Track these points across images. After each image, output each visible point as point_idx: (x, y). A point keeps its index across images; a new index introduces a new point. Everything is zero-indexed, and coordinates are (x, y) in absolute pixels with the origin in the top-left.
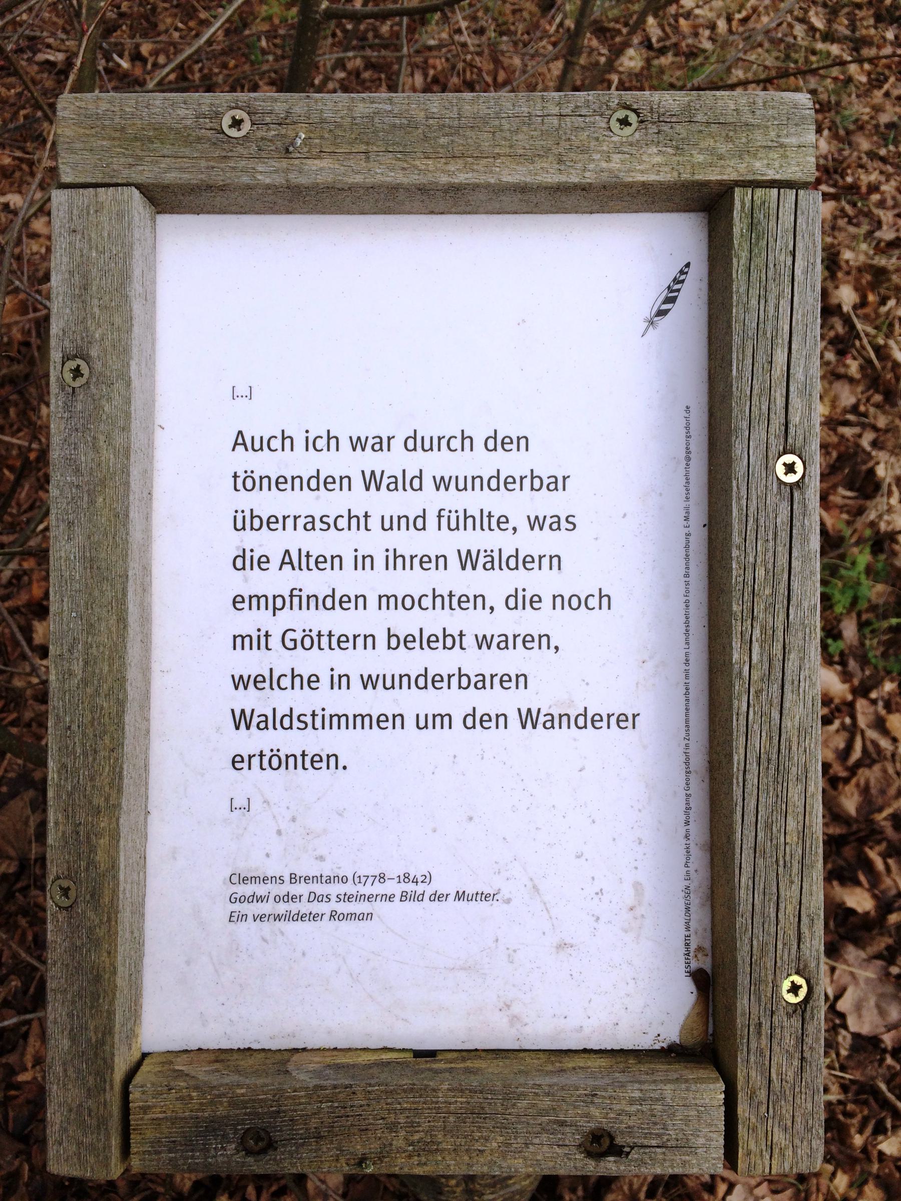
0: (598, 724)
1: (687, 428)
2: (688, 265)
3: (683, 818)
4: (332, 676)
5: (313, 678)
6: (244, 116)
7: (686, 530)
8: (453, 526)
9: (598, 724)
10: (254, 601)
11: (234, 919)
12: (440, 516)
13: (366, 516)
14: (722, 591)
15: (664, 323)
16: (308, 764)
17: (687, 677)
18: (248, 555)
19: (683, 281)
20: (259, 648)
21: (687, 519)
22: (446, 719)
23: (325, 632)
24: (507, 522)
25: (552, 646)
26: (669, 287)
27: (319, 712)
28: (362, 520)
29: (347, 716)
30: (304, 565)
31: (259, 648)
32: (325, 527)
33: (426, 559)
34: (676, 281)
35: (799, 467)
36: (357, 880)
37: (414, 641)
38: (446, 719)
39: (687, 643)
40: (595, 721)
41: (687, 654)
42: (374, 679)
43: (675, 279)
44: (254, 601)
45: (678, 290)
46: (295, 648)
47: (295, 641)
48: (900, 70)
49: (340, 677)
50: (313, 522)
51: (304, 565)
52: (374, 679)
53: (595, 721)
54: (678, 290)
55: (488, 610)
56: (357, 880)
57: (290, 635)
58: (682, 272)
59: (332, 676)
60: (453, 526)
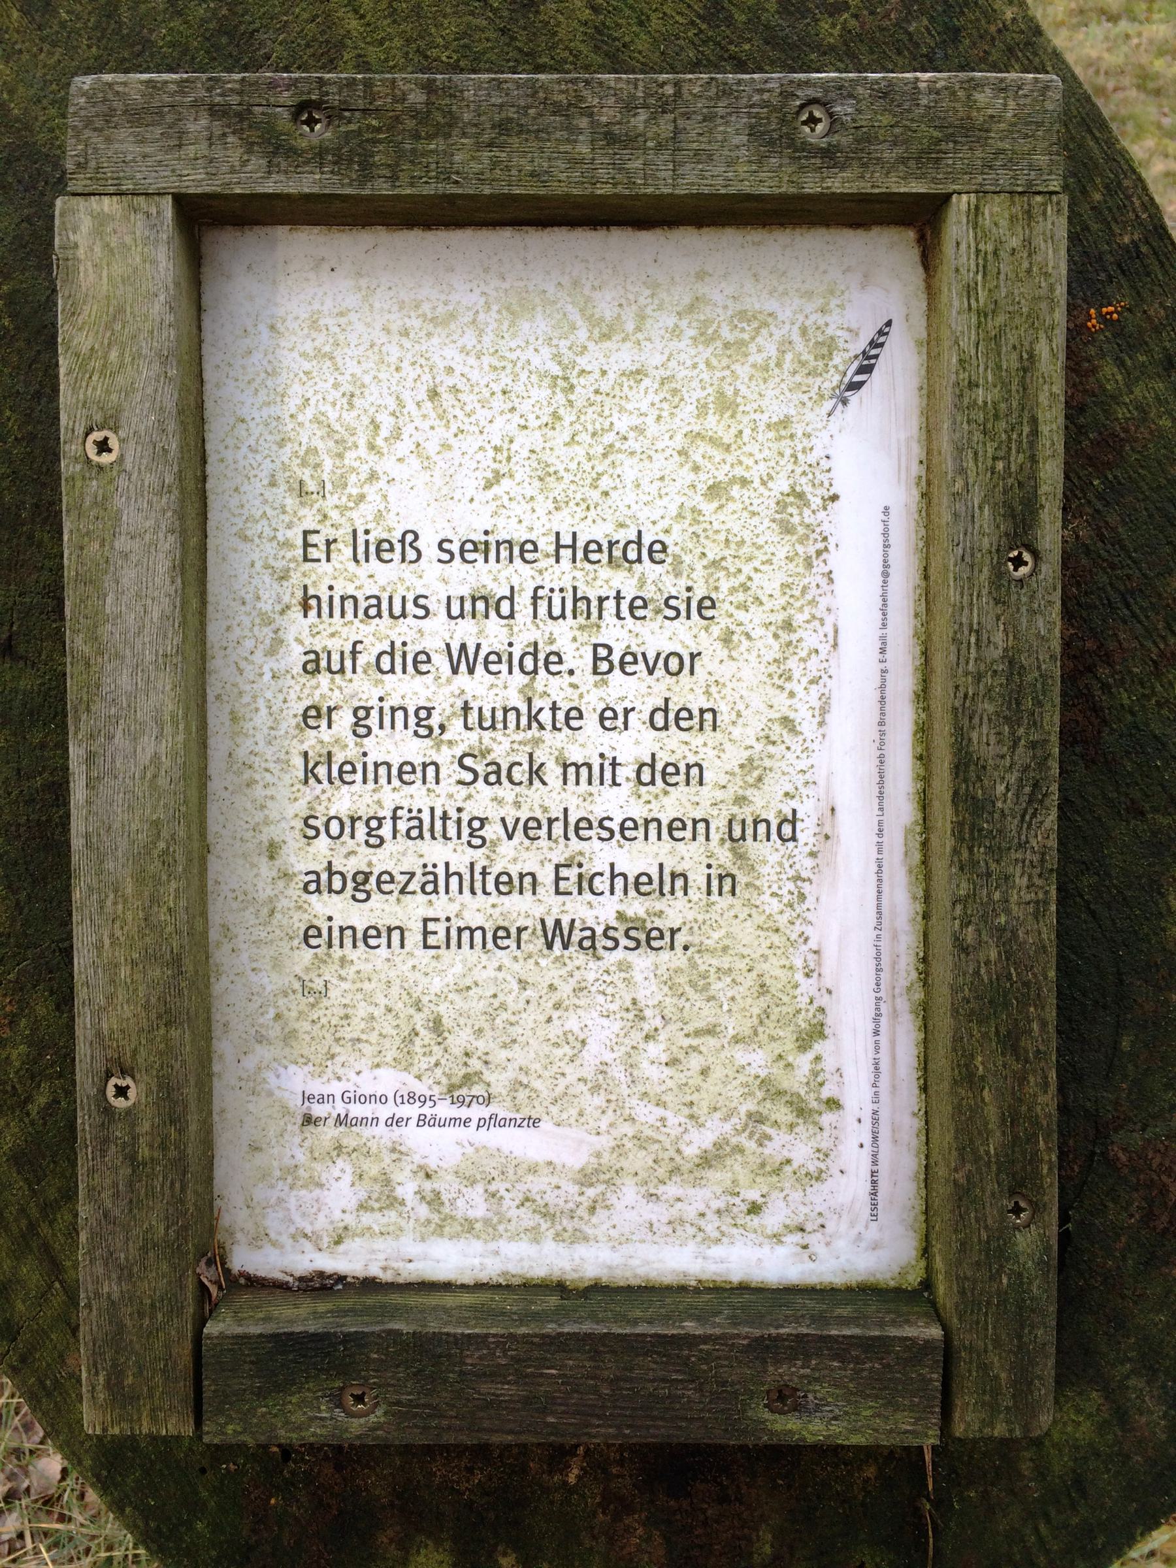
1: (886, 533)
2: (889, 324)
3: (871, 1026)
4: (709, 876)
7: (882, 666)
8: (556, 611)
11: (570, 885)
12: (535, 598)
14: (920, 758)
15: (854, 398)
16: (490, 887)
17: (880, 852)
19: (882, 345)
21: (883, 651)
24: (560, 662)
26: (864, 352)
27: (453, 814)
30: (478, 885)
32: (632, 944)
34: (874, 344)
35: (111, 1091)
36: (399, 1100)
39: (881, 809)
40: (883, 698)
41: (880, 823)
42: (471, 651)
43: (871, 343)
45: (876, 357)
48: (1175, 134)
51: (478, 885)
52: (471, 651)
53: (883, 698)
54: (876, 357)
56: (399, 1100)
58: (881, 333)
59: (709, 876)
60: (556, 611)
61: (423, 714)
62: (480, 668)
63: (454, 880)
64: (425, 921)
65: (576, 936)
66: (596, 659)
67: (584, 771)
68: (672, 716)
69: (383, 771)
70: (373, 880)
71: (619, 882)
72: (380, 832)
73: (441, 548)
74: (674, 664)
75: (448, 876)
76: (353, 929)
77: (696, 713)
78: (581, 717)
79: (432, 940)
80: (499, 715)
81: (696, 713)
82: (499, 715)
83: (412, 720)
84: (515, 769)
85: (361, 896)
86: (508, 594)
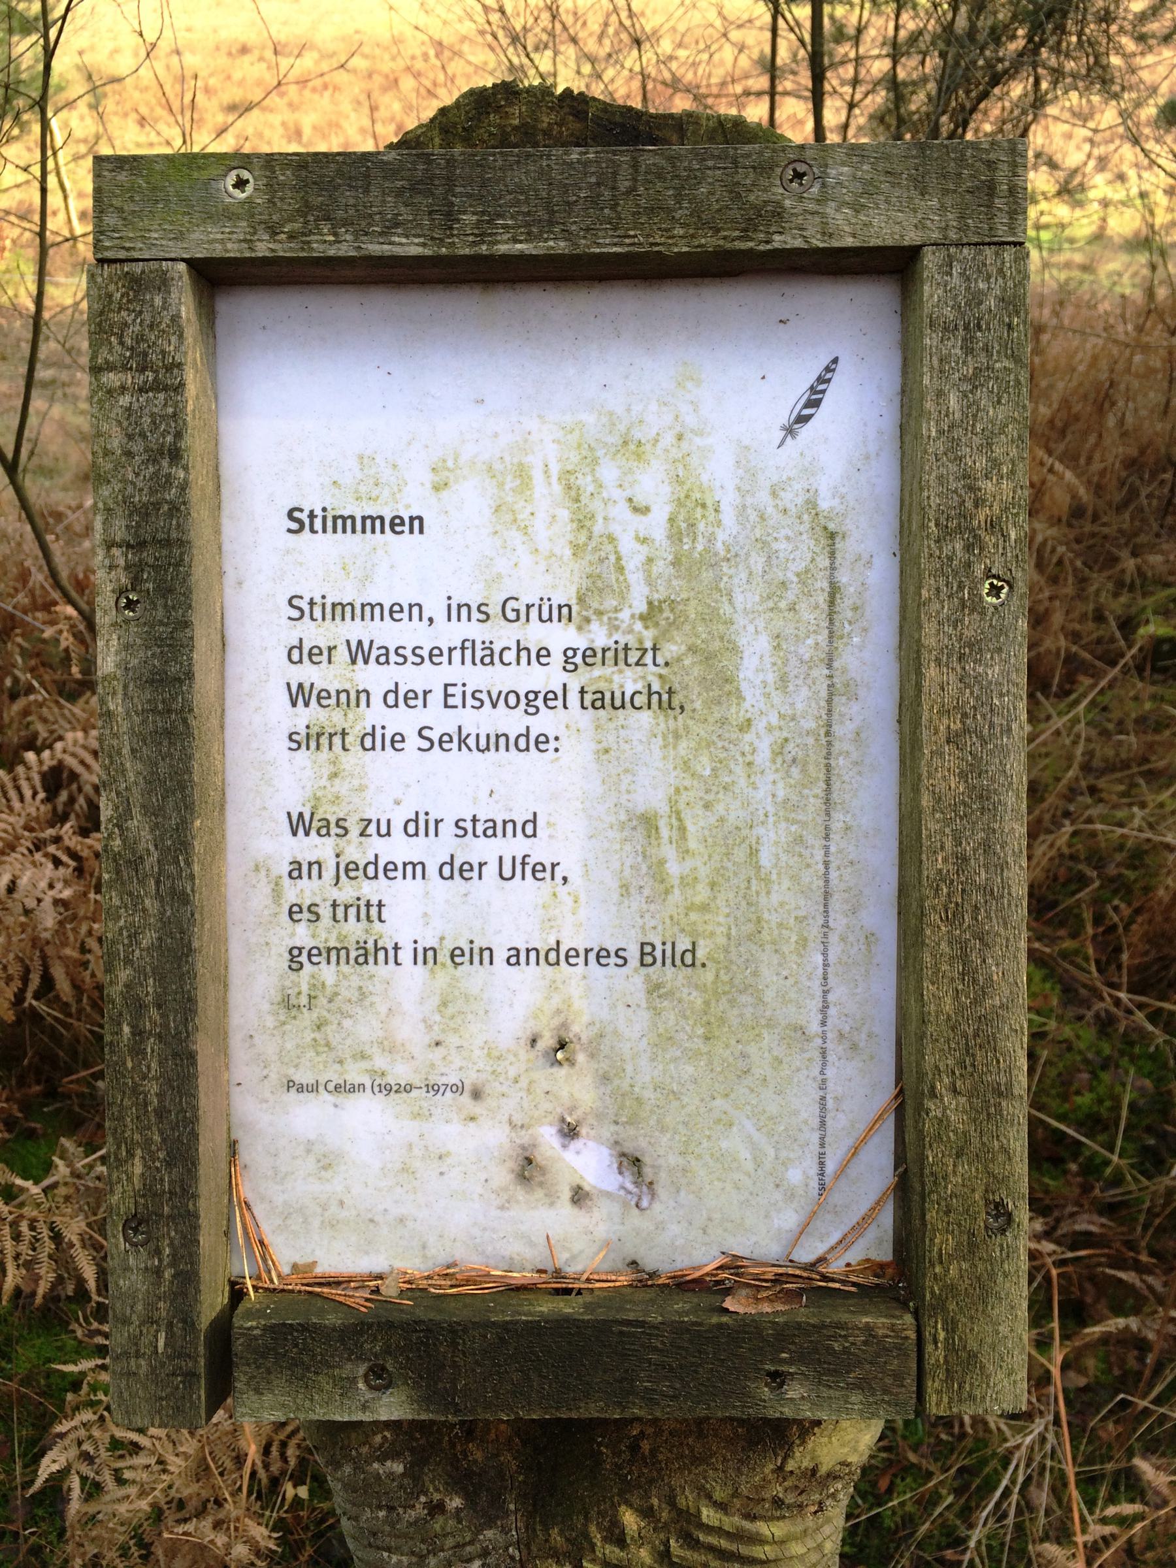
0: (412, 703)
2: (835, 361)
5: (398, 738)
6: (234, 173)
7: (821, 1093)
8: (545, 616)
9: (412, 703)
10: (409, 868)
11: (457, 701)
13: (396, 948)
18: (422, 818)
19: (829, 381)
20: (427, 835)
22: (419, 868)
23: (374, 902)
25: (425, 616)
26: (812, 388)
28: (391, 953)
29: (381, 605)
31: (427, 835)
33: (539, 868)
34: (821, 380)
37: (556, 698)
38: (419, 868)
42: (307, 818)
44: (409, 868)
45: (823, 392)
46: (518, 619)
47: (518, 611)
49: (425, 950)
50: (387, 655)
55: (426, 621)
57: (511, 604)
58: (828, 369)
60: (545, 616)
61: (531, 696)
62: (313, 833)
63: (381, 954)
64: (446, 686)
65: (315, 824)
66: (643, 954)
67: (377, 610)
68: (305, 652)
69: (502, 740)
70: (541, 696)
71: (524, 654)
72: (575, 660)
73: (291, 740)
74: (512, 700)
75: (376, 950)
76: (506, 736)
77: (333, 694)
78: (549, 655)
79: (451, 701)
80: (493, 740)
81: (333, 694)
82: (493, 740)
83: (523, 701)
84: (636, 697)
85: (570, 667)
86: (296, 643)
